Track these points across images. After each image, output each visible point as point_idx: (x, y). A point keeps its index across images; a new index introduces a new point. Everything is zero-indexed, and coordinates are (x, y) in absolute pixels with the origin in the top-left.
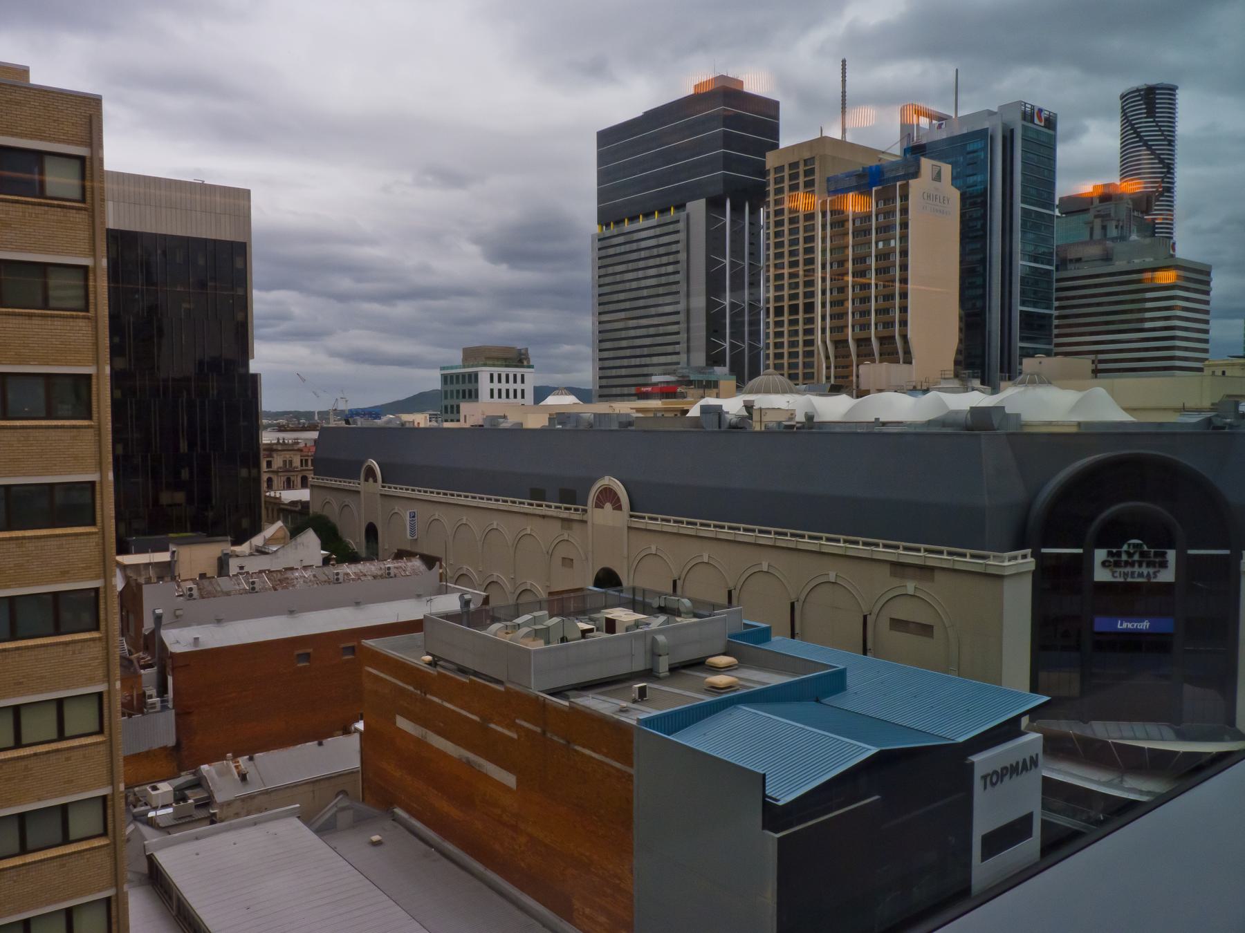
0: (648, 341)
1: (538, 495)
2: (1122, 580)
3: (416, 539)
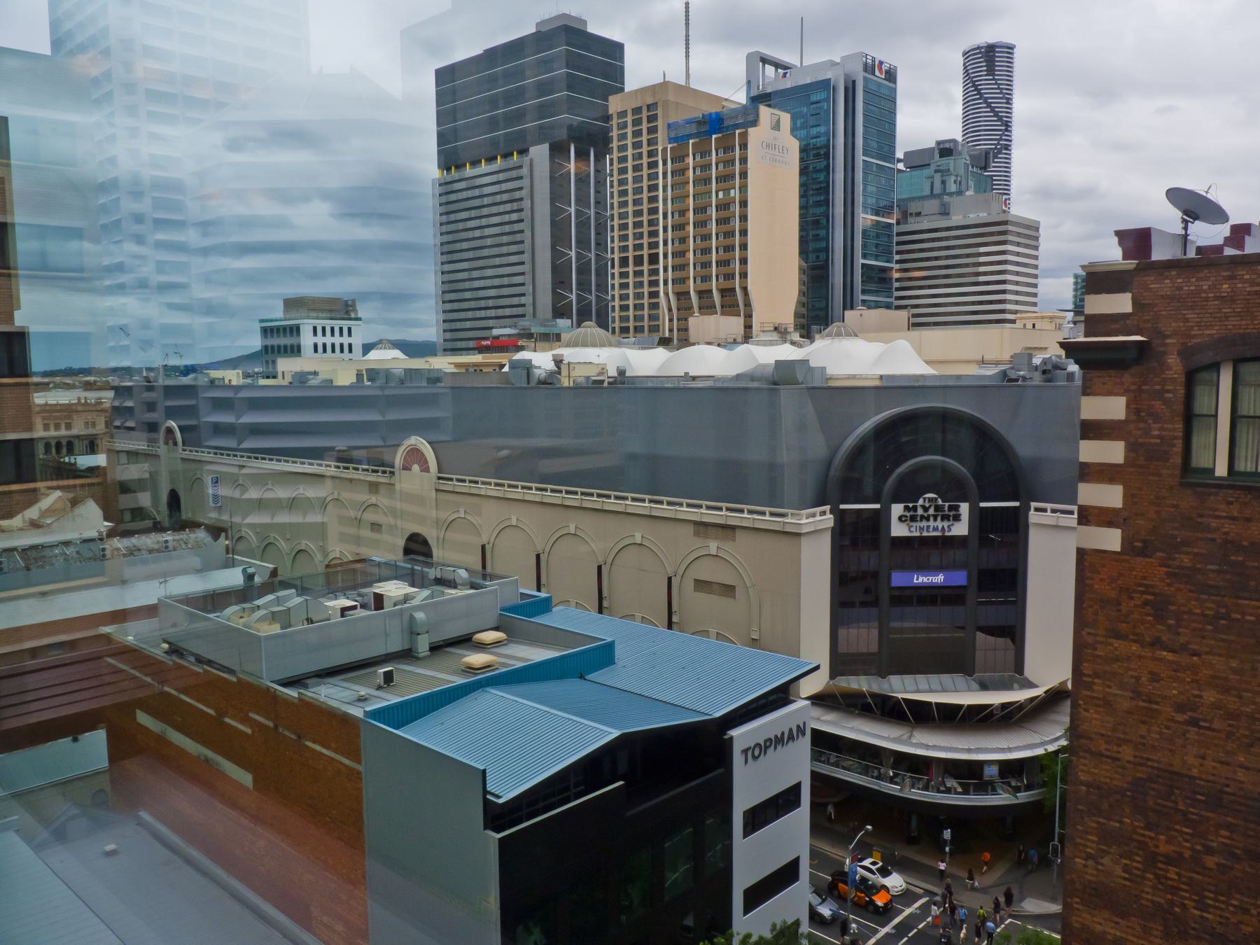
0: (492, 293)
3: (221, 506)
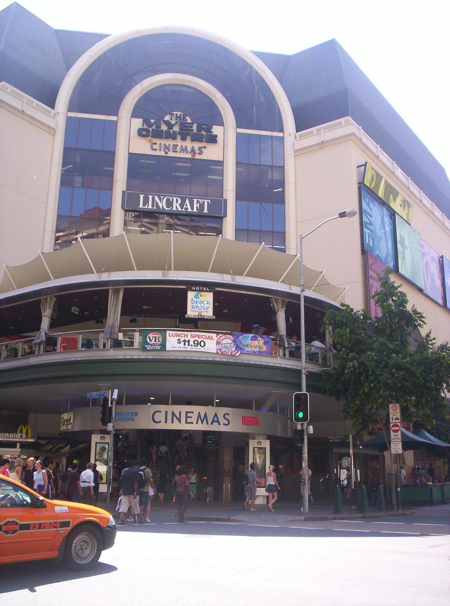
2: (162, 153)
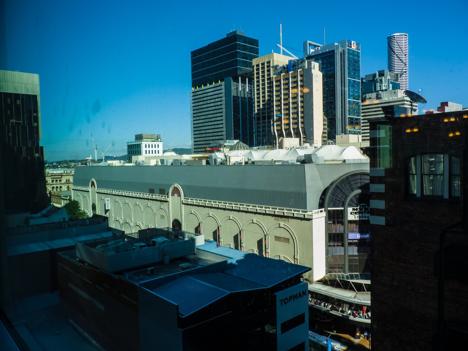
1: (152, 191)
